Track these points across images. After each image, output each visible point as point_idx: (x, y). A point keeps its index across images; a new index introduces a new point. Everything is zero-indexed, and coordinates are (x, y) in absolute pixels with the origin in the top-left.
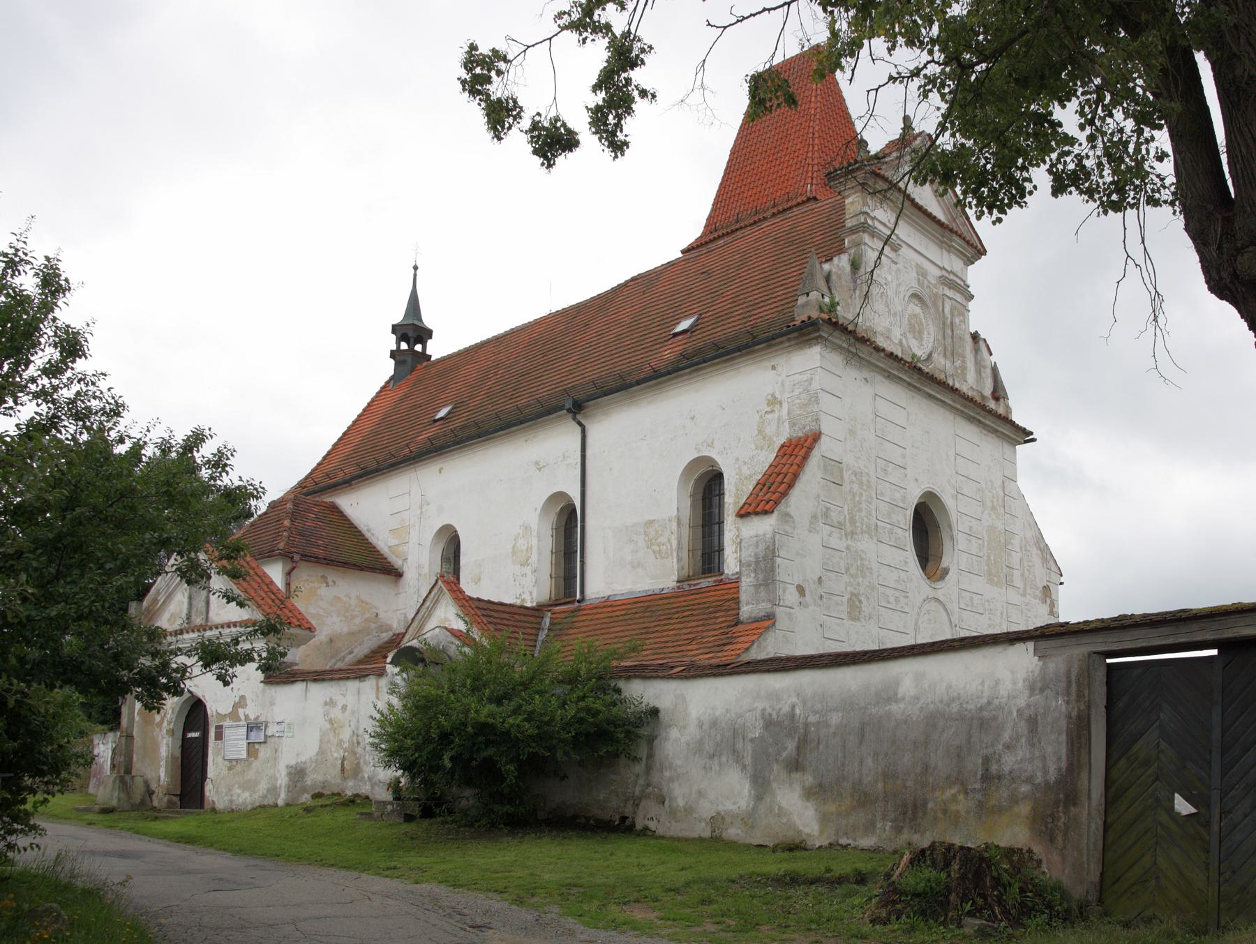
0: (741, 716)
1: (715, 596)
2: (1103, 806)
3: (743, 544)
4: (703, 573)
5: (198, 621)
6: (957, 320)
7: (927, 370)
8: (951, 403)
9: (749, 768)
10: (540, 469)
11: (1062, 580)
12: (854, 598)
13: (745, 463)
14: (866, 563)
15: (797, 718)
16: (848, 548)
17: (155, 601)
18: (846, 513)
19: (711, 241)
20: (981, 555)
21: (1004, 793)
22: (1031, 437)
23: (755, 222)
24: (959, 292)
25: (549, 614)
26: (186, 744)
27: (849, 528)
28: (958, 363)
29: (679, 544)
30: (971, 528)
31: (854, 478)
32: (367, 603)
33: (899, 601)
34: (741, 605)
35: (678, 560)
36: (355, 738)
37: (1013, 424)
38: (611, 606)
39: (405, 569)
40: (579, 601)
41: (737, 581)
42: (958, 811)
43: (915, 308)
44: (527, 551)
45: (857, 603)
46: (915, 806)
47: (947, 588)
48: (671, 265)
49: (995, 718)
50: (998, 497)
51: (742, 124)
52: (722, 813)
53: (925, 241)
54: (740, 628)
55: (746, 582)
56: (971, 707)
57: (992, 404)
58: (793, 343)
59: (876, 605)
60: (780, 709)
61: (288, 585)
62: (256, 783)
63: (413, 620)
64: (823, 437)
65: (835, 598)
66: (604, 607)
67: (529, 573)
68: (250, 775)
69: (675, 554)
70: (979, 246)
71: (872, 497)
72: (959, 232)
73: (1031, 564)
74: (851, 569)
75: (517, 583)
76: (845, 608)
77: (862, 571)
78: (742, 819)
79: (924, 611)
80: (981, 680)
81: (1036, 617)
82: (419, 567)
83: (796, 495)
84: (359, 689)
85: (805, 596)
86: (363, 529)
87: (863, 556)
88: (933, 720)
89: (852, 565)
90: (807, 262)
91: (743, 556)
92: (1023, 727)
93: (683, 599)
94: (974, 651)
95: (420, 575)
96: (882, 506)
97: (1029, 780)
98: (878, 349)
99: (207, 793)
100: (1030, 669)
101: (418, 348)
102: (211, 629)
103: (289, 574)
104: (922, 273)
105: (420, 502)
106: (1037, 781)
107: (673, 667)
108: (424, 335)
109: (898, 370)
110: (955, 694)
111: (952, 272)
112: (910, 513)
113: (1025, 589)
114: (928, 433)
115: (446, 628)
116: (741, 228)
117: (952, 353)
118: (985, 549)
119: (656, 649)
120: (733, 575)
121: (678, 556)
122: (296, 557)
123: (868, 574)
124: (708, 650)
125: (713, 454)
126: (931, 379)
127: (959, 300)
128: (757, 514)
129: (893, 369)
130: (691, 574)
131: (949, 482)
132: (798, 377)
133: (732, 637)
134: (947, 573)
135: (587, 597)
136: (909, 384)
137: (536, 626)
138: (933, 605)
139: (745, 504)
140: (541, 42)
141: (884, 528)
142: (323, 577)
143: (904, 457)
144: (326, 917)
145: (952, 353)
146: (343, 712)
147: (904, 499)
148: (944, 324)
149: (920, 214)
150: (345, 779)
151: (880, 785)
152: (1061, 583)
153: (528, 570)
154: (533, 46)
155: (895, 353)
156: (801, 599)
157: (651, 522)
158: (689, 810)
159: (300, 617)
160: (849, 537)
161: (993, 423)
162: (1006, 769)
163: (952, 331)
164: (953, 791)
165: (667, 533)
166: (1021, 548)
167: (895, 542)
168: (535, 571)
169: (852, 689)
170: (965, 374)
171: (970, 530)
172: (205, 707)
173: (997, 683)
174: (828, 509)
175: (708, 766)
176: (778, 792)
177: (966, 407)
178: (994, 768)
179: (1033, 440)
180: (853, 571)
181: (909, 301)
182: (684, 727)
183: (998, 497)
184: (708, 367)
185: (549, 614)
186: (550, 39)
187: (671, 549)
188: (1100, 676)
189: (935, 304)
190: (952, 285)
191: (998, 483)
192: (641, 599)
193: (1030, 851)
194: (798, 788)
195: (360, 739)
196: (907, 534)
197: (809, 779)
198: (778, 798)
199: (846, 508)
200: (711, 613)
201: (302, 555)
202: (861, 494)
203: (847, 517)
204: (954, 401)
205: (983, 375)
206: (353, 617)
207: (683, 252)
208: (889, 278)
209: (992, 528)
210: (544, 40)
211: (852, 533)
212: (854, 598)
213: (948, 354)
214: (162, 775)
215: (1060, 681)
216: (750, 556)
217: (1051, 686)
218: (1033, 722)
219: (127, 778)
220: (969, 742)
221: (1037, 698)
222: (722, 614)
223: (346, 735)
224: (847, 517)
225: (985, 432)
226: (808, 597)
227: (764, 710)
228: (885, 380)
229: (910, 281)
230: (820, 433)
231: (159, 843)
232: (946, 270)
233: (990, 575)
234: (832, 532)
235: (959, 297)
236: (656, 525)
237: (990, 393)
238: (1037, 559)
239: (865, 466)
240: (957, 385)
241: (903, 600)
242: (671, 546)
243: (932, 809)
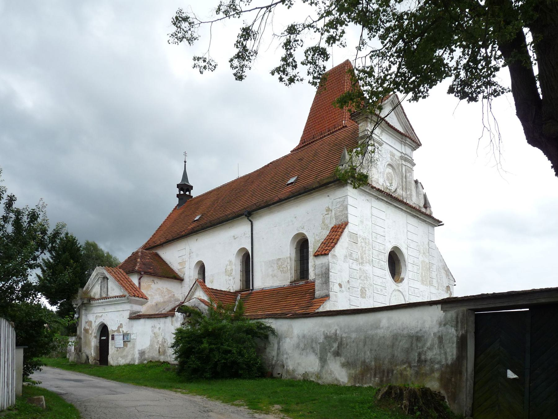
0: (315, 334)
1: (305, 288)
2: (473, 375)
3: (316, 267)
5: (104, 296)
6: (408, 175)
7: (394, 196)
8: (405, 209)
9: (319, 354)
10: (235, 239)
11: (455, 283)
12: (363, 289)
13: (317, 235)
14: (368, 275)
15: (337, 335)
16: (360, 269)
17: (88, 288)
18: (359, 255)
19: (303, 147)
20: (419, 273)
21: (428, 368)
22: (441, 223)
23: (321, 138)
24: (409, 163)
25: (240, 295)
26: (101, 341)
27: (360, 261)
28: (408, 193)
29: (291, 268)
31: (363, 241)
32: (170, 291)
34: (316, 291)
36: (164, 340)
37: (433, 218)
39: (185, 278)
40: (251, 290)
41: (314, 282)
42: (407, 375)
43: (390, 170)
44: (231, 271)
45: (364, 291)
46: (388, 373)
47: (403, 286)
48: (286, 157)
49: (423, 336)
50: (426, 249)
51: (315, 97)
52: (308, 372)
53: (394, 141)
54: (315, 300)
57: (423, 210)
59: (372, 292)
60: (331, 331)
61: (139, 283)
62: (127, 356)
63: (187, 296)
64: (349, 224)
65: (354, 289)
66: (261, 292)
67: (232, 279)
68: (125, 353)
69: (289, 271)
70: (418, 142)
71: (370, 248)
72: (409, 137)
75: (227, 283)
76: (359, 293)
77: (366, 278)
78: (316, 375)
79: (393, 295)
82: (190, 277)
83: (338, 246)
85: (342, 288)
87: (367, 272)
88: (395, 337)
89: (362, 276)
90: (342, 153)
91: (316, 272)
92: (436, 341)
93: (292, 289)
94: (413, 308)
95: (190, 280)
96: (375, 252)
97: (439, 363)
98: (373, 187)
99: (109, 360)
101: (188, 193)
102: (109, 298)
103: (140, 279)
104: (393, 155)
105: (189, 252)
106: (443, 363)
107: (287, 314)
108: (190, 188)
109: (381, 196)
110: (406, 326)
111: (406, 154)
112: (387, 255)
114: (394, 222)
115: (198, 299)
116: (315, 141)
117: (405, 188)
118: (420, 270)
119: (282, 308)
121: (290, 272)
122: (142, 273)
123: (369, 280)
124: (302, 309)
126: (396, 200)
127: (409, 166)
128: (322, 255)
129: (379, 195)
130: (296, 279)
131: (404, 242)
132: (339, 200)
133: (312, 304)
134: (403, 280)
135: (254, 289)
136: (387, 202)
137: (234, 299)
138: (397, 293)
139: (317, 251)
140: (208, 22)
141: (376, 261)
142: (153, 280)
144: (148, 405)
145: (405, 188)
146: (159, 330)
147: (384, 249)
148: (402, 176)
149: (389, 128)
150: (160, 355)
151: (373, 363)
152: (455, 285)
153: (231, 278)
154: (204, 23)
155: (380, 189)
156: (341, 289)
157: (280, 259)
159: (142, 294)
160: (361, 265)
161: (424, 218)
162: (429, 358)
163: (406, 179)
165: (286, 264)
166: (437, 270)
168: (234, 278)
169: (361, 323)
170: (412, 197)
171: (414, 262)
174: (351, 253)
175: (301, 353)
176: (330, 364)
177: (412, 211)
178: (423, 357)
179: (443, 225)
180: (362, 278)
181: (387, 167)
182: (292, 338)
183: (426, 249)
184: (301, 197)
185: (240, 295)
186: (212, 22)
187: (288, 270)
188: (472, 319)
189: (398, 168)
190: (406, 160)
191: (426, 243)
192: (278, 289)
193: (439, 393)
195: (166, 340)
196: (386, 264)
197: (343, 360)
198: (330, 367)
199: (359, 253)
200: (304, 294)
201: (145, 272)
202: (366, 247)
203: (360, 257)
204: (406, 209)
205: (420, 198)
206: (165, 296)
207: (291, 152)
209: (423, 262)
210: (209, 22)
211: (362, 263)
212: (363, 289)
213: (404, 189)
214: (93, 353)
215: (453, 321)
216: (319, 272)
217: (449, 323)
218: (441, 339)
219: (80, 353)
220: (412, 346)
221: (442, 328)
222: (308, 295)
223: (160, 339)
224: (360, 257)
225: (421, 222)
226: (343, 288)
227: (324, 331)
228: (376, 201)
230: (348, 222)
231: (90, 377)
232: (403, 153)
233: (423, 281)
235: (409, 165)
236: (281, 260)
237: (423, 205)
238: (444, 275)
240: (408, 202)
242: (288, 268)
243: (395, 373)
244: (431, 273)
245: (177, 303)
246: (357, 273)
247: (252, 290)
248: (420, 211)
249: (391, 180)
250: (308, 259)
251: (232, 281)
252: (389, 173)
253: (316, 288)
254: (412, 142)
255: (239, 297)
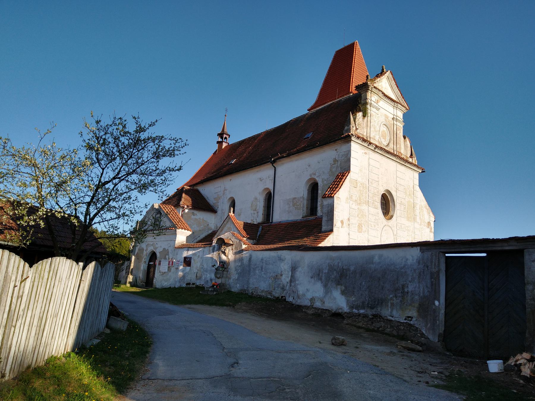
3: (324, 207)
4: (311, 215)
10: (261, 181)
16: (358, 208)
18: (358, 197)
26: (149, 267)
30: (401, 202)
33: (375, 226)
35: (303, 211)
38: (281, 225)
39: (218, 210)
44: (256, 206)
52: (314, 297)
55: (324, 219)
56: (398, 267)
58: (342, 142)
66: (279, 225)
67: (256, 213)
73: (423, 214)
74: (359, 215)
77: (363, 216)
80: (401, 259)
81: (425, 233)
84: (204, 250)
86: (206, 197)
89: (359, 214)
100: (418, 256)
112: (380, 197)
113: (421, 223)
118: (406, 209)
120: (320, 216)
125: (315, 177)
131: (394, 186)
134: (392, 217)
135: (274, 222)
143: (378, 178)
147: (378, 192)
157: (295, 198)
158: (304, 295)
160: (359, 205)
164: (391, 296)
166: (420, 209)
167: (375, 206)
172: (156, 254)
173: (407, 260)
180: (360, 216)
188: (443, 260)
194: (339, 290)
196: (379, 204)
199: (358, 195)
202: (363, 191)
208: (375, 119)
214: (141, 276)
224: (358, 198)
226: (344, 225)
227: (329, 263)
229: (382, 119)
234: (353, 203)
239: (365, 181)
241: (377, 226)
244: (416, 211)
245: (210, 231)
246: (356, 212)
247: (272, 222)
248: (407, 161)
249: (385, 137)
250: (317, 199)
251: (256, 215)
252: (384, 131)
253: (323, 224)
254: (402, 107)
255: (260, 228)
